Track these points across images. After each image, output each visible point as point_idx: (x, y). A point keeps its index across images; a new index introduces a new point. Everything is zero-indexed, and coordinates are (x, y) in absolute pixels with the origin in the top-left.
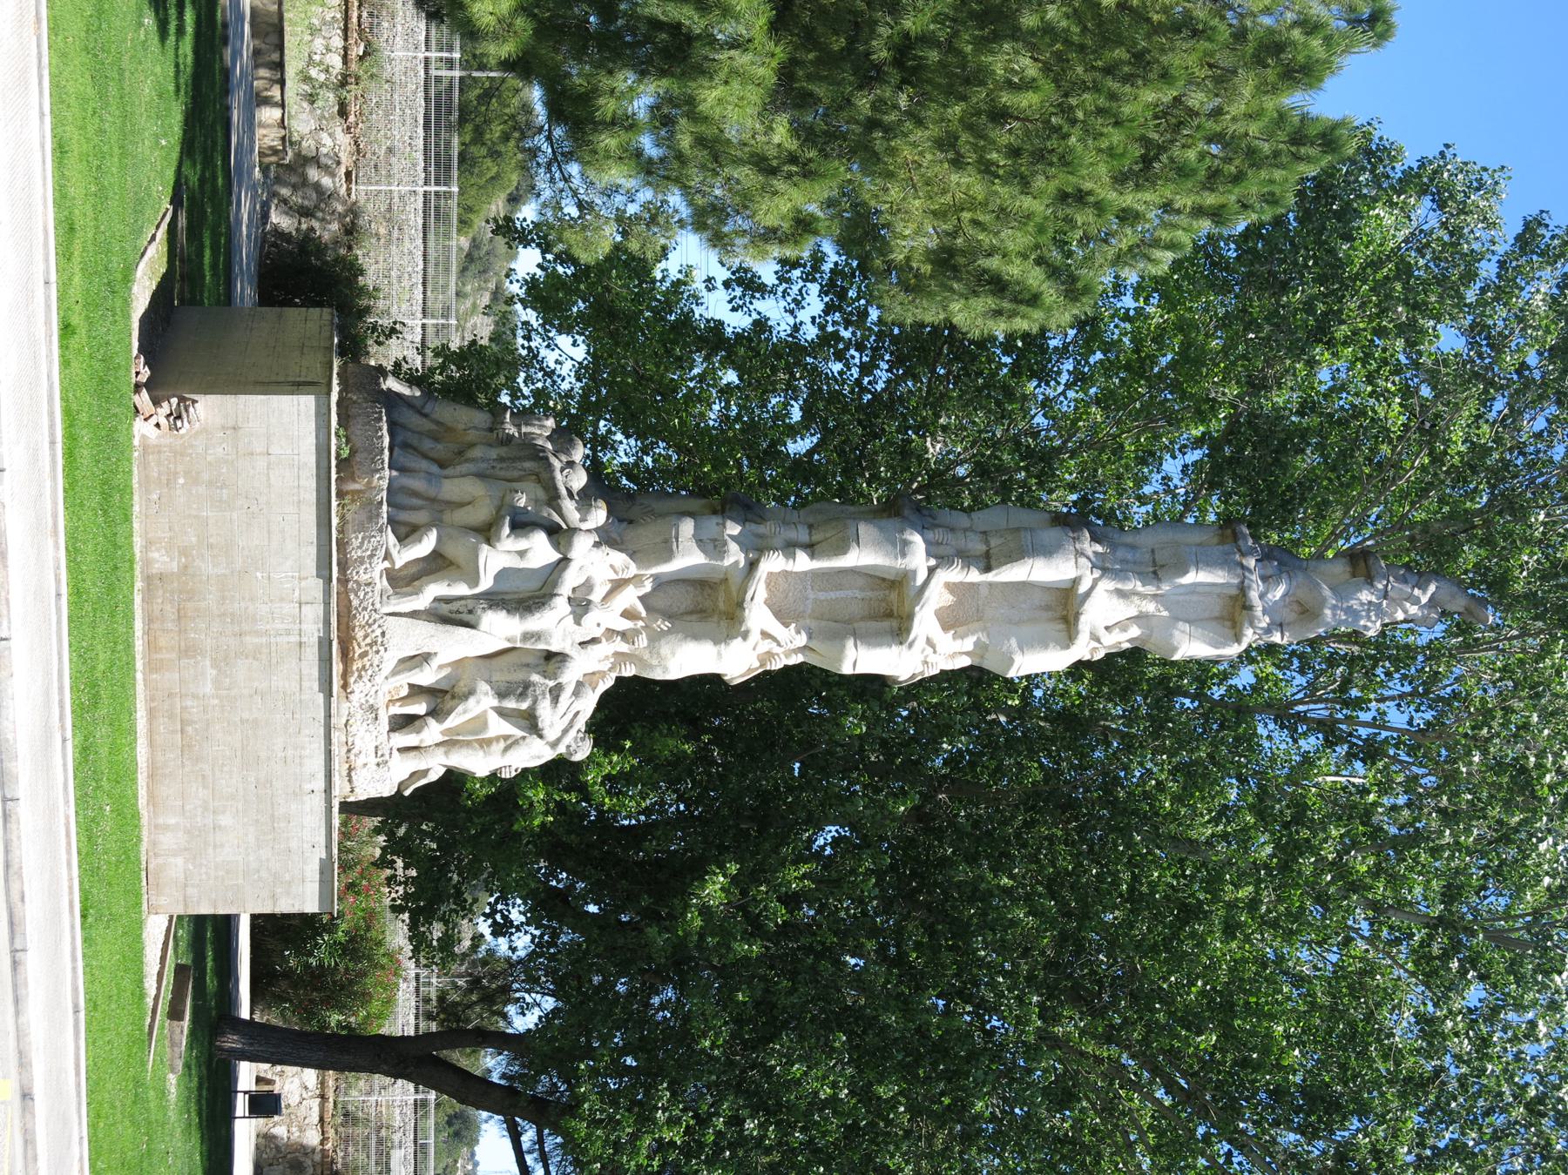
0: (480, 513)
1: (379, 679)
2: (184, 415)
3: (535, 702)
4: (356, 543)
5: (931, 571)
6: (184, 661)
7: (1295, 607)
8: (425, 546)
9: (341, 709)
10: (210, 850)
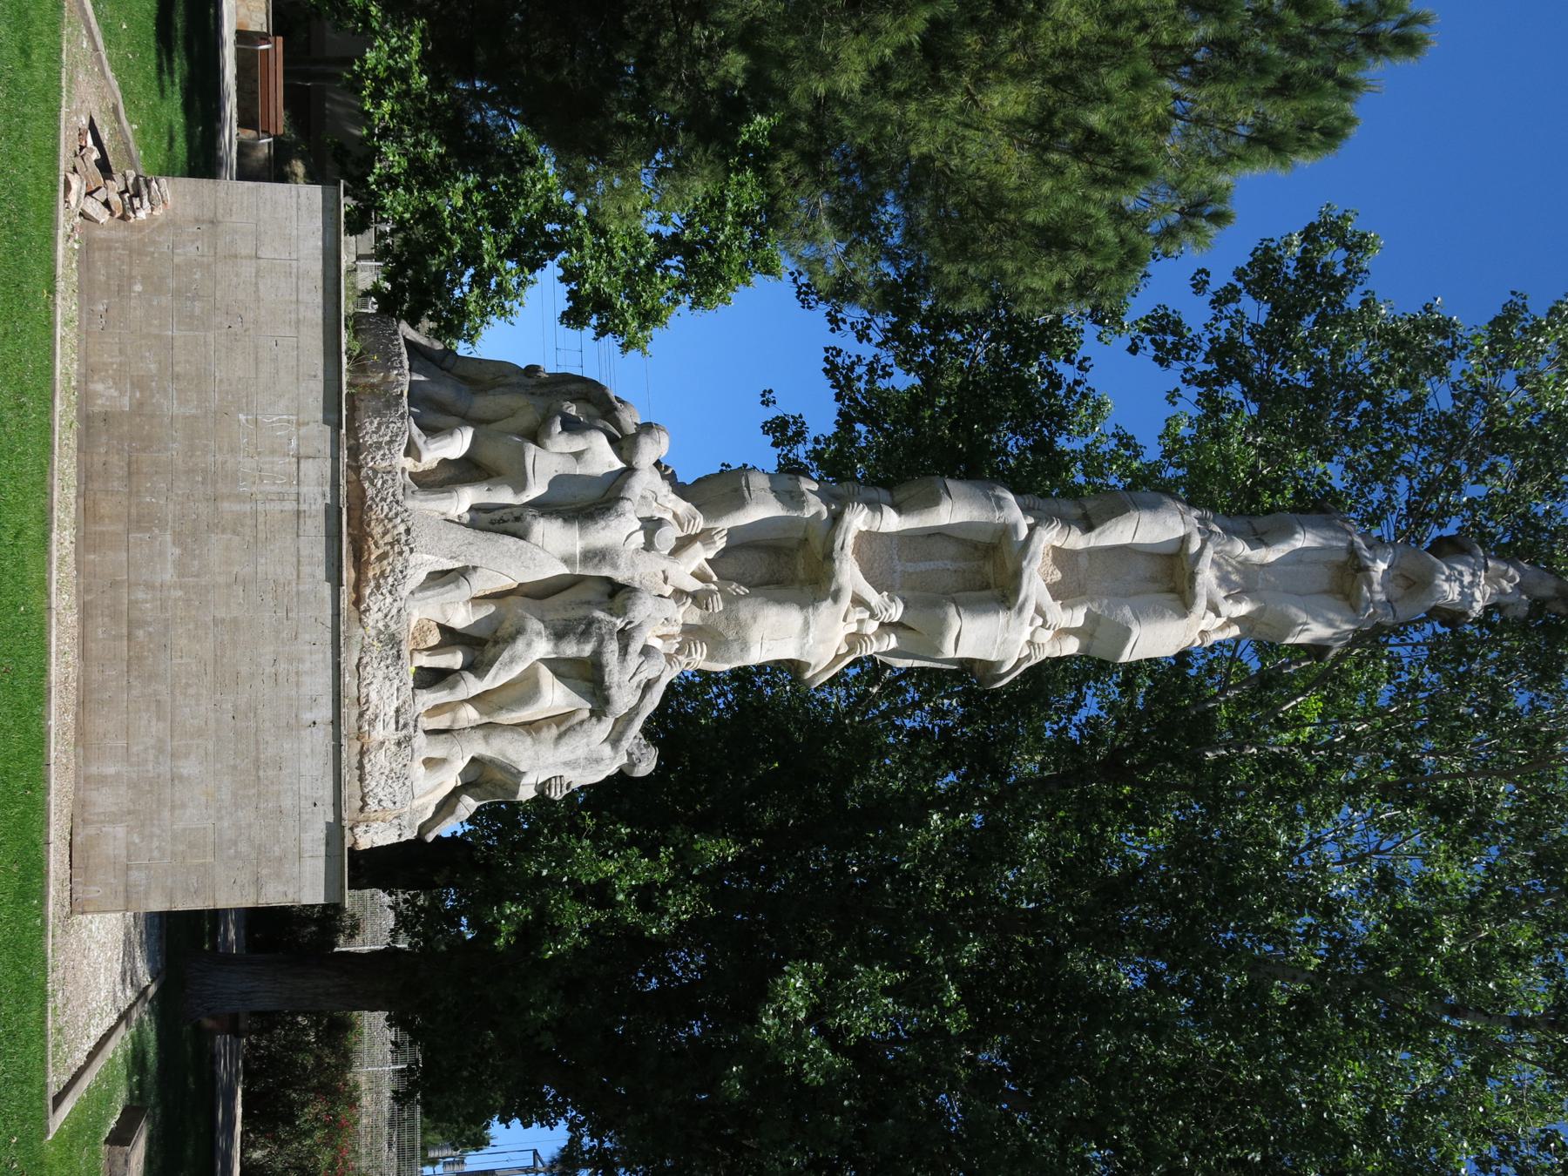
0: (527, 419)
1: (404, 592)
2: (144, 192)
3: (601, 642)
4: (370, 428)
5: (1032, 528)
6: (134, 536)
7: (1401, 581)
8: (457, 445)
9: (355, 635)
10: (166, 814)
